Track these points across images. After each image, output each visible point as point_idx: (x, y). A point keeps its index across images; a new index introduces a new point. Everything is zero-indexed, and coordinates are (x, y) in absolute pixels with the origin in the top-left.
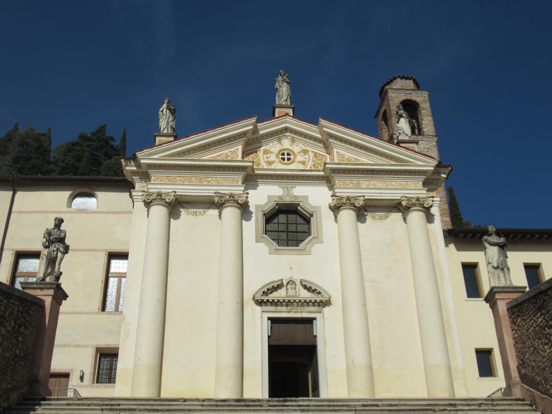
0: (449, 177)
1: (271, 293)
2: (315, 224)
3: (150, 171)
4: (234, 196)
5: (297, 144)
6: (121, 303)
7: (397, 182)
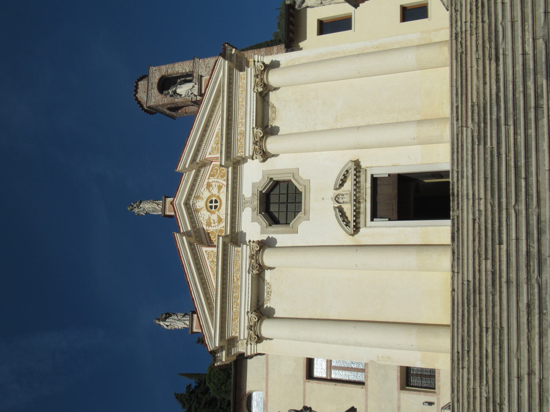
0: (235, 47)
1: (347, 218)
3: (226, 337)
4: (252, 255)
5: (201, 194)
6: (357, 366)
7: (240, 96)
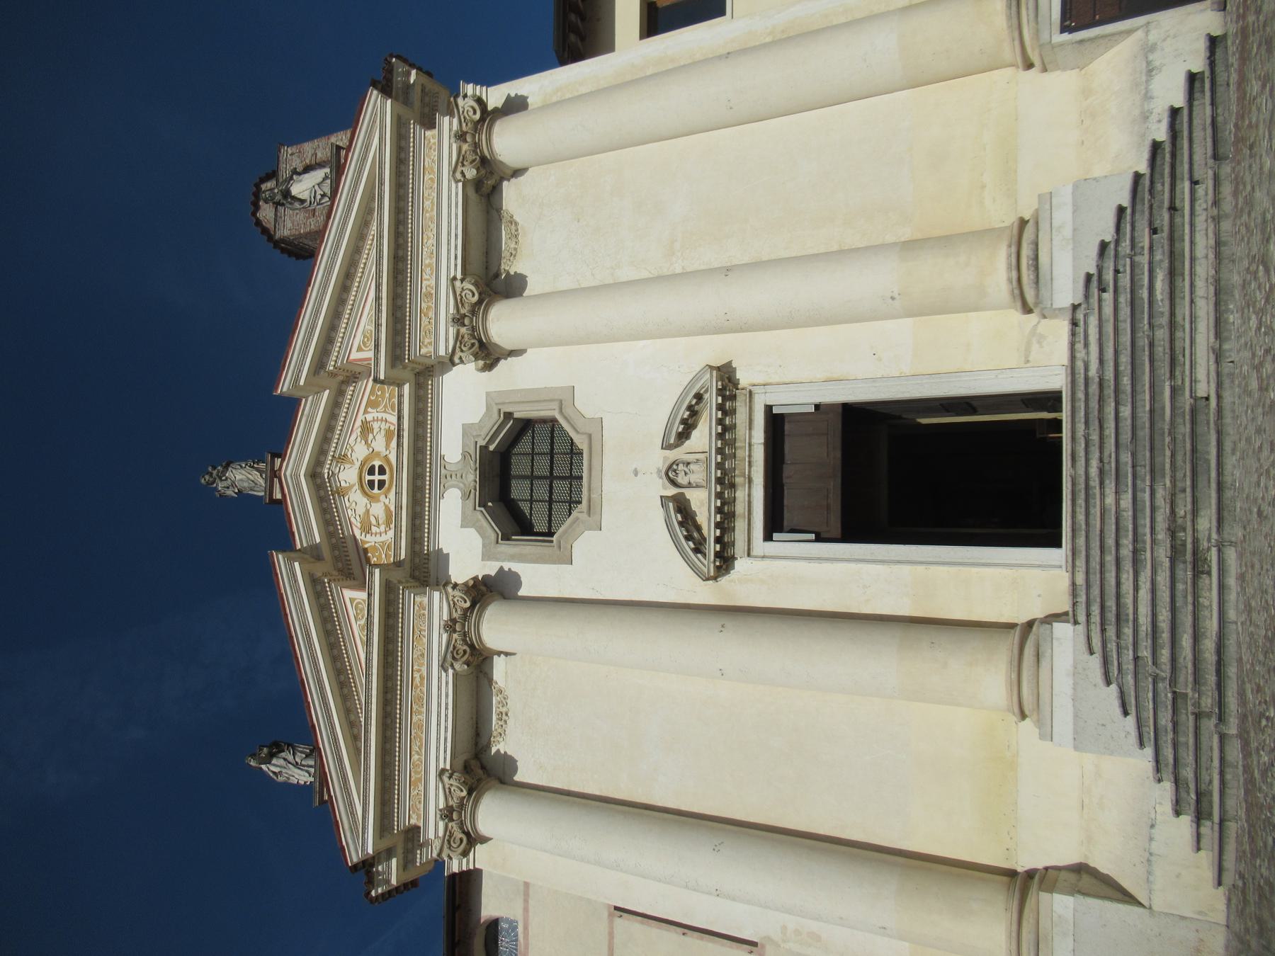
1: (699, 529)
2: (528, 409)
5: (350, 450)
